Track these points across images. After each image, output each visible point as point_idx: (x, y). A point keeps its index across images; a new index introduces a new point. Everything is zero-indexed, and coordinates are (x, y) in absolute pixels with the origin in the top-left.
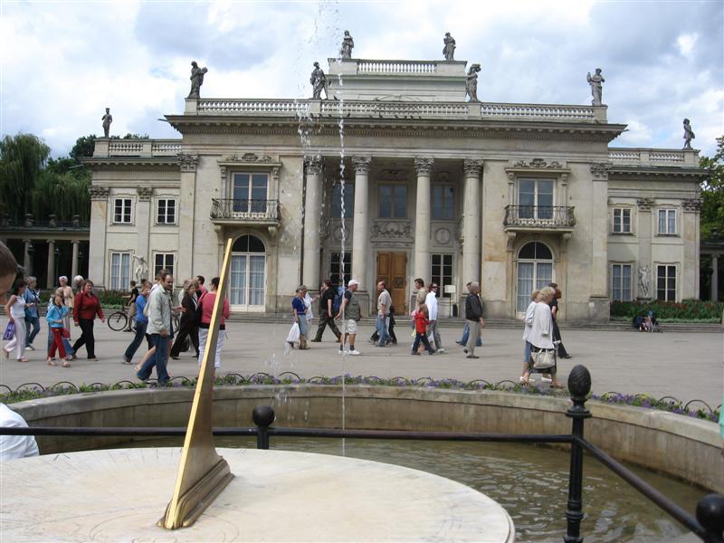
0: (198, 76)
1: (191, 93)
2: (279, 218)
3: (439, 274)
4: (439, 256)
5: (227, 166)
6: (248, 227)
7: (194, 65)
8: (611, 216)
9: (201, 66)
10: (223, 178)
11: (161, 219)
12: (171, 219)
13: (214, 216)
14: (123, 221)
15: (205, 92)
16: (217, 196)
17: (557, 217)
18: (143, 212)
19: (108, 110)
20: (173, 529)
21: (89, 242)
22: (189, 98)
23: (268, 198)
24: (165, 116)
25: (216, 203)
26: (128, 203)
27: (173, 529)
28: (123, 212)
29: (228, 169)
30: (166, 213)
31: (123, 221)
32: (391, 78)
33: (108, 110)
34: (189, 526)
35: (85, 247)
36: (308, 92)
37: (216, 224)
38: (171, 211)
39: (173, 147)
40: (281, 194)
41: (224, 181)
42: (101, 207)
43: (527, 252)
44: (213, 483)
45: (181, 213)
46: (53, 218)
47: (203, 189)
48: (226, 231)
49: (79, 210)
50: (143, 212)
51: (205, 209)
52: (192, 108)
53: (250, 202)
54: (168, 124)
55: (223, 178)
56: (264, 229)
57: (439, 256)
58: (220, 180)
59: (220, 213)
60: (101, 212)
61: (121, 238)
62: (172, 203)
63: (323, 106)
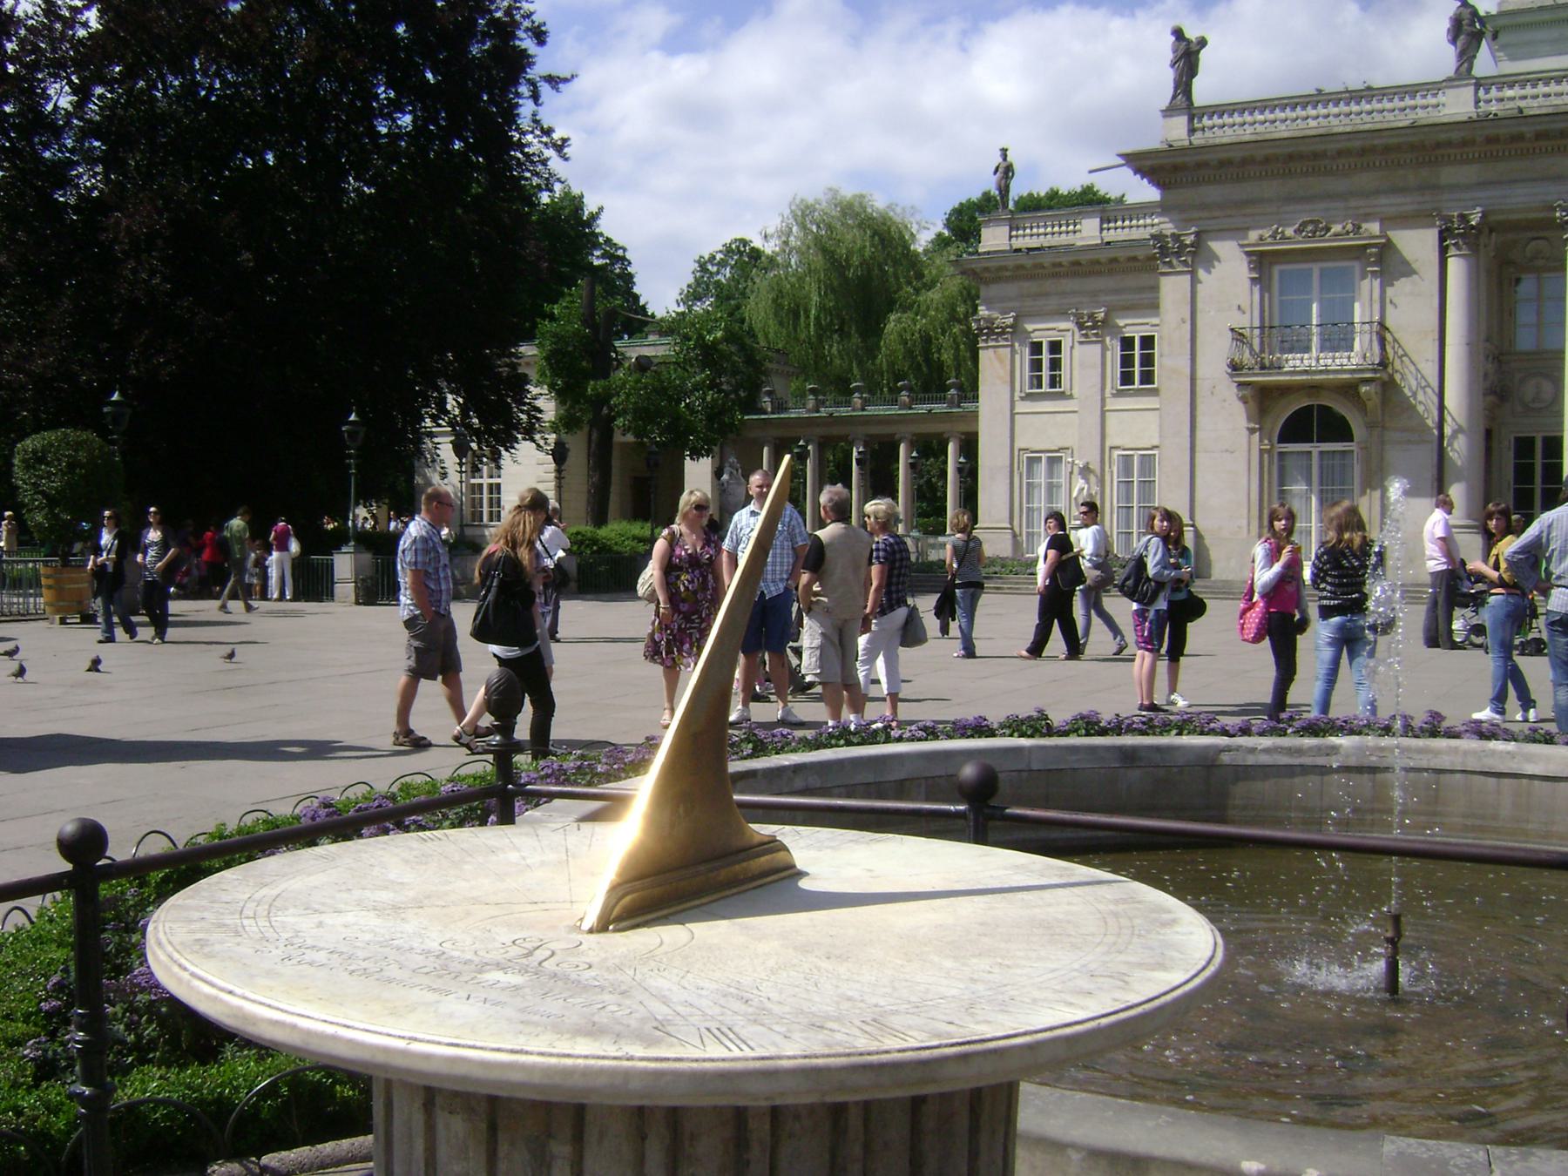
0: (1187, 57)
1: (1174, 97)
2: (1384, 363)
3: (1543, 490)
4: (1531, 440)
5: (1262, 254)
6: (1313, 388)
7: (1178, 34)
8: (1161, 366)
9: (1191, 34)
10: (1253, 279)
11: (1127, 378)
12: (1147, 378)
13: (1235, 367)
14: (1045, 388)
15: (1204, 90)
16: (1242, 321)
17: (1357, 357)
18: (1086, 364)
19: (1004, 151)
20: (591, 931)
21: (976, 434)
22: (1169, 112)
23: (1357, 319)
24: (1121, 156)
25: (1238, 336)
26: (1055, 347)
27: (591, 931)
28: (1046, 372)
29: (1262, 262)
30: (1137, 367)
31: (1045, 388)
32: (1547, 16)
33: (1004, 151)
34: (615, 931)
35: (970, 447)
36: (1445, 59)
37: (1240, 384)
38: (1148, 360)
39: (1149, 221)
40: (1389, 307)
41: (1256, 289)
42: (1001, 361)
43: (1298, 429)
44: (724, 874)
45: (1170, 361)
46: (857, 389)
47: (1214, 304)
48: (1262, 399)
49: (945, 374)
50: (1086, 364)
51: (1216, 353)
52: (1177, 130)
53: (1315, 330)
54: (1127, 172)
55: (1253, 279)
56: (1348, 389)
57: (1531, 440)
58: (1247, 283)
59: (1247, 358)
60: (997, 369)
61: (1046, 426)
62: (1148, 342)
63: (1481, 92)
